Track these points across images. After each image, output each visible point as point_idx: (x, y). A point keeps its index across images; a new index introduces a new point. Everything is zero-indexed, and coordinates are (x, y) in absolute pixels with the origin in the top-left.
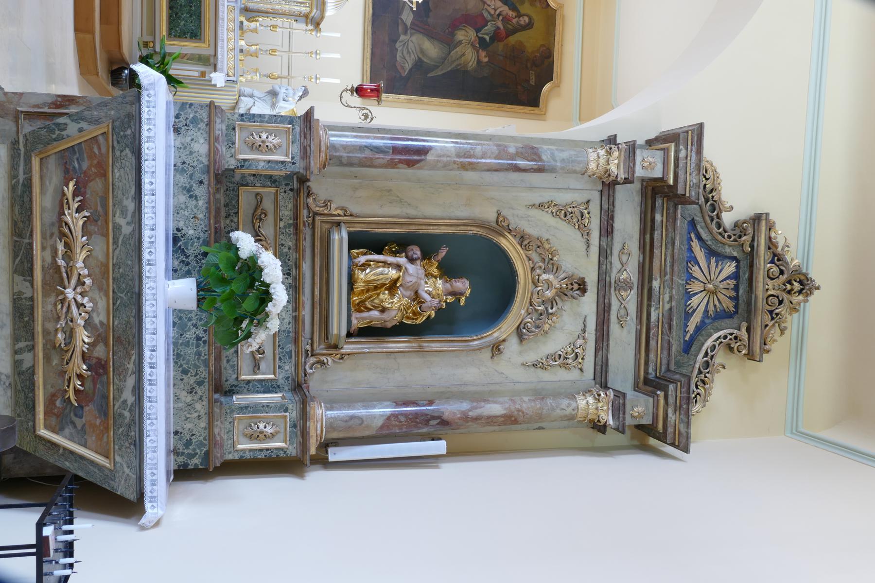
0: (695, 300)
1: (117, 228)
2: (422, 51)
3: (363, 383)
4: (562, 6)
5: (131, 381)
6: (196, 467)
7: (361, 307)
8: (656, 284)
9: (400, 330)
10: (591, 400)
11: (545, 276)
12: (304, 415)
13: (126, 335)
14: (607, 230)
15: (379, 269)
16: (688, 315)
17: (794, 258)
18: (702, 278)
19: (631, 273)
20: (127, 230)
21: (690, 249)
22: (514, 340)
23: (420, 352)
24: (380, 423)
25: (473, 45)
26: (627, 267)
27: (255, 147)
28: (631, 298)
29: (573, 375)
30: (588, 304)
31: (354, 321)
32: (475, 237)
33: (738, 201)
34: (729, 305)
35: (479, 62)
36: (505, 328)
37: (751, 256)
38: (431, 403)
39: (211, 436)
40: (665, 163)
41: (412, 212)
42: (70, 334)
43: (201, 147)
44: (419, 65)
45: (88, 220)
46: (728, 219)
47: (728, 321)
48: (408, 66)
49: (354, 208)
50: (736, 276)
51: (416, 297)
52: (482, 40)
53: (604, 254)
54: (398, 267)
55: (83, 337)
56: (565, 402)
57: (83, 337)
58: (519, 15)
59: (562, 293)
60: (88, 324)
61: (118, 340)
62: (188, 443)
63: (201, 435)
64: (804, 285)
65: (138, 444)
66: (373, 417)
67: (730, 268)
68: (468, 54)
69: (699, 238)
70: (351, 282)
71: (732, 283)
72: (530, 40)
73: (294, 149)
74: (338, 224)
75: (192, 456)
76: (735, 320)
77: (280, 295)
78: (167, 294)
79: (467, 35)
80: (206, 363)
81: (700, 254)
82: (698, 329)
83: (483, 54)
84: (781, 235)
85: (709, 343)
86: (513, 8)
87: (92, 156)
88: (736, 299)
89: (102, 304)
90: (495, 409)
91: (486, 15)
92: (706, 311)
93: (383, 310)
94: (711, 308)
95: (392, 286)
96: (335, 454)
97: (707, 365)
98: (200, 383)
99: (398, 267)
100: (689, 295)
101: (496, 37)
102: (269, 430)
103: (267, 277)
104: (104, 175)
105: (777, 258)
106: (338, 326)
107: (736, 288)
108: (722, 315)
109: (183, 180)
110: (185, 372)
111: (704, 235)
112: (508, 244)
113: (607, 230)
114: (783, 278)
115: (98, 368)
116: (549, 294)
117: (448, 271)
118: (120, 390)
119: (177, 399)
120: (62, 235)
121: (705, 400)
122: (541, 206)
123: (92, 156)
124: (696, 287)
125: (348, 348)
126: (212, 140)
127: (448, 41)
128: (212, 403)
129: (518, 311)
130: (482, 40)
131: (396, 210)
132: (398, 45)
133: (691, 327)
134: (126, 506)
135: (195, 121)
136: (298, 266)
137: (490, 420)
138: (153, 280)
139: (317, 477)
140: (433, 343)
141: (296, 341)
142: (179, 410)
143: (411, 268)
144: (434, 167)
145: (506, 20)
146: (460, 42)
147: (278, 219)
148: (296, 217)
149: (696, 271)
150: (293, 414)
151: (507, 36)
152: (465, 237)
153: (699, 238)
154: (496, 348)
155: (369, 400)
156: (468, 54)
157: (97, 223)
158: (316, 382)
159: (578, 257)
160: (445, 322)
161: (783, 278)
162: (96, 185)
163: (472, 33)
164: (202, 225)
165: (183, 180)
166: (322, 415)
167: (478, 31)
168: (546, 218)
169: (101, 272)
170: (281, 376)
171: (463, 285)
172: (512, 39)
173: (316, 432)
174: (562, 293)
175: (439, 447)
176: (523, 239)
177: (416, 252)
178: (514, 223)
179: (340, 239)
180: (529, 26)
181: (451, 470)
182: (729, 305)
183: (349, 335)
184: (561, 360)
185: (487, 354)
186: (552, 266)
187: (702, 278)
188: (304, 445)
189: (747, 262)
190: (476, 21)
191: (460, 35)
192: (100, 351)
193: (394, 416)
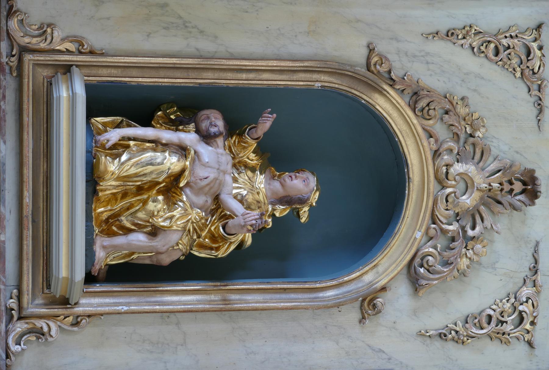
7: (112, 226)
9: (187, 269)
11: (458, 168)
15: (146, 154)
22: (402, 288)
23: (225, 310)
32: (327, 93)
36: (386, 266)
41: (206, 46)
49: (96, 39)
51: (217, 208)
54: (182, 150)
59: (492, 200)
74: (67, 69)
93: (155, 232)
95: (171, 187)
99: (182, 150)
106: (69, 265)
112: (390, 107)
116: (468, 201)
117: (276, 157)
122: (450, 34)
125: (88, 304)
129: (409, 233)
131: (175, 42)
140: (249, 294)
143: (206, 152)
154: (369, 304)
160: (271, 255)
171: (304, 184)
174: (492, 200)
177: (215, 121)
179: (70, 97)
185: (354, 314)
186: (471, 146)
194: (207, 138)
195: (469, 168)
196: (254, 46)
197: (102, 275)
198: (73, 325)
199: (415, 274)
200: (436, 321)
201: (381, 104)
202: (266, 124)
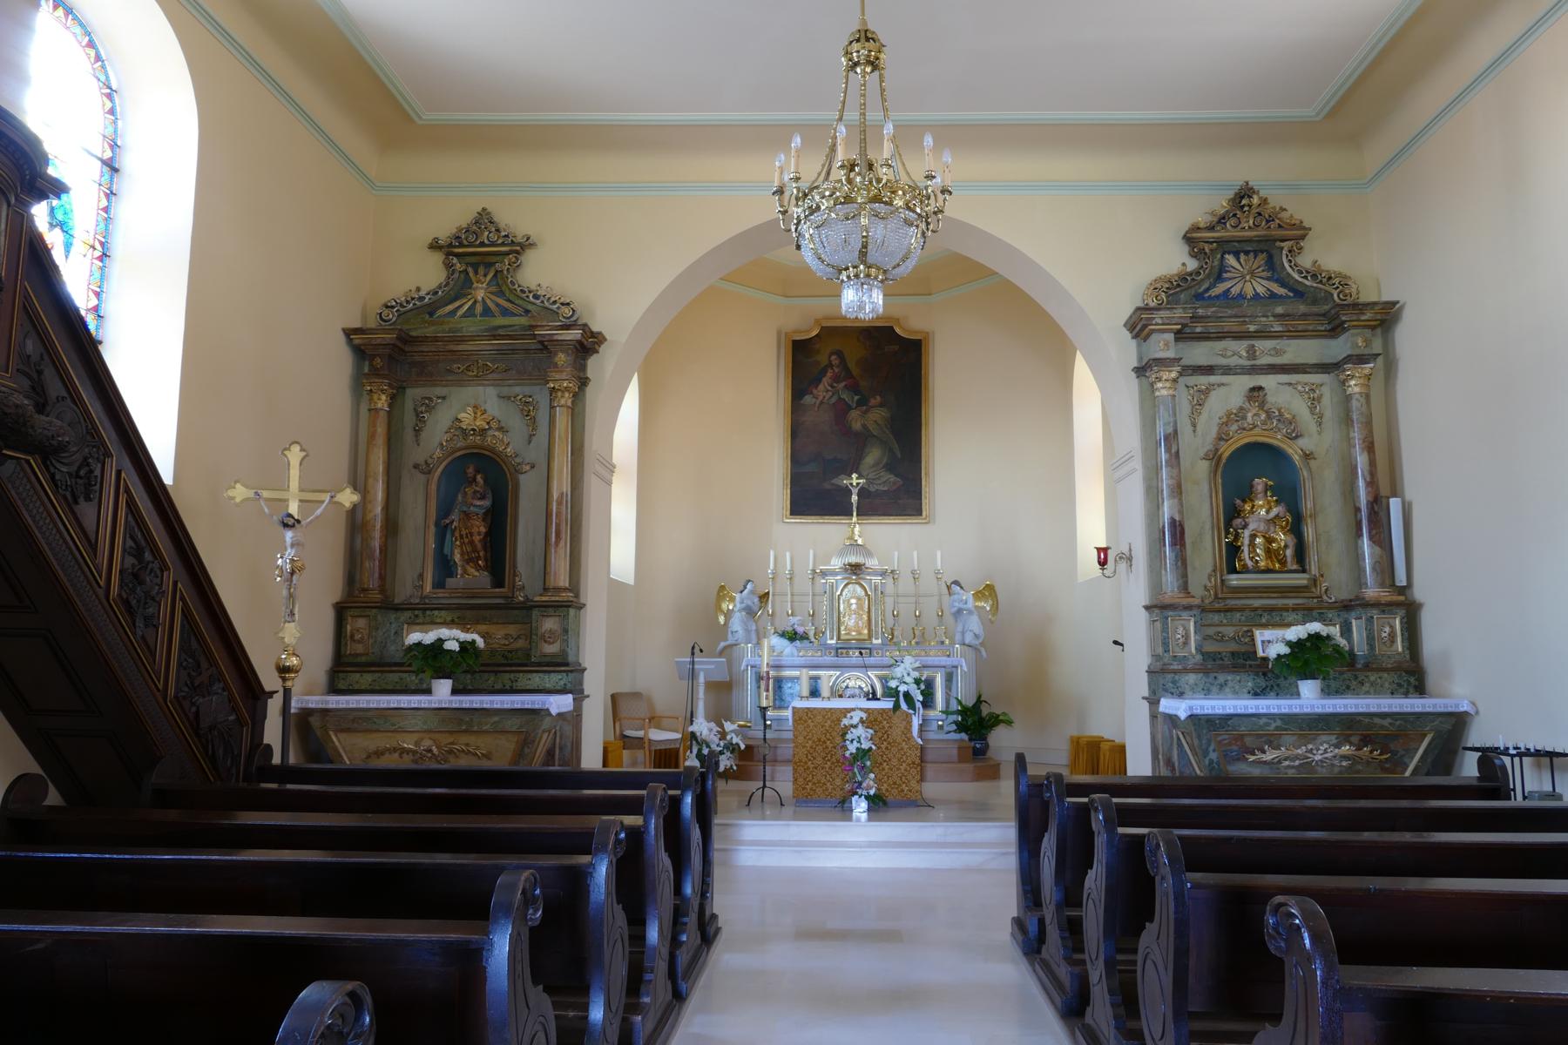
0: (1260, 290)
1: (1277, 728)
2: (876, 464)
3: (1336, 557)
4: (817, 321)
5: (1377, 720)
6: (1413, 676)
7: (1283, 562)
8: (1252, 328)
9: (1296, 528)
10: (1353, 383)
11: (1249, 419)
12: (1376, 605)
13: (1346, 725)
14: (1209, 370)
15: (1254, 552)
16: (1273, 295)
17: (1221, 203)
18: (1240, 285)
19: (1241, 347)
20: (1279, 723)
21: (1217, 297)
22: (1300, 442)
23: (1314, 516)
24: (1377, 549)
25: (865, 412)
26: (1235, 351)
27: (1186, 643)
28: (1262, 345)
29: (1326, 393)
30: (1268, 382)
31: (1295, 567)
32: (1223, 472)
33: (1175, 260)
34: (1262, 257)
35: (881, 405)
36: (1293, 451)
37: (1220, 242)
38: (1358, 510)
39: (1392, 670)
40: (1163, 331)
41: (1208, 526)
42: (1344, 757)
43: (1192, 678)
44: (890, 468)
45: (1270, 743)
46: (1192, 265)
47: (1276, 259)
48: (892, 478)
49: (1209, 569)
50: (1237, 255)
51: (1273, 521)
52: (860, 403)
53: (1228, 371)
54: (1253, 537)
55: (1346, 749)
56: (1354, 404)
57: (1346, 749)
58: (830, 365)
59: (1262, 405)
60: (1337, 746)
61: (1349, 728)
62: (1400, 685)
63: (1394, 677)
64: (1245, 192)
65: (1419, 715)
66: (1372, 555)
67: (1231, 260)
68: (874, 418)
69: (1208, 290)
70: (1268, 571)
71: (1242, 257)
72: (855, 353)
73: (1185, 615)
74: (1223, 581)
75: (1409, 683)
76: (1274, 252)
77: (1315, 627)
78: (1309, 697)
79: (856, 421)
80: (1341, 673)
81: (1220, 288)
82: (1283, 285)
83: (873, 402)
84: (1202, 220)
85: (1296, 276)
86: (823, 372)
87: (1230, 744)
88: (1256, 253)
89: (1324, 738)
90: (1361, 460)
91: (834, 400)
92: (1267, 279)
93: (1286, 546)
94: (1264, 274)
95: (1269, 540)
96: (1401, 580)
97: (1314, 276)
98: (1356, 678)
99: (1253, 537)
100: (1256, 296)
101: (854, 388)
102: (1387, 629)
103: (1303, 635)
104: (1242, 736)
105: (1222, 220)
106: (1300, 580)
107: (1247, 253)
108: (1272, 265)
109: (1215, 689)
110: (1348, 687)
111: (1206, 285)
112: (1227, 450)
113: (1209, 370)
114: (1239, 213)
115: (1366, 740)
116: (1263, 416)
117: (1248, 495)
118: (1382, 727)
119: (1368, 693)
120: (1280, 762)
121: (1346, 277)
122: (1194, 425)
123: (1230, 744)
124: (1249, 292)
125: (1314, 570)
126: (1186, 671)
127: (861, 441)
128: (1373, 670)
129: (1277, 440)
130: (860, 403)
131: (1208, 537)
132: (872, 489)
133: (1282, 291)
134: (1458, 722)
135: (1174, 682)
136: (1256, 609)
137: (1372, 463)
138: (1301, 706)
139: (1419, 593)
140: (1307, 506)
141: (1311, 609)
142: (1377, 691)
143: (1252, 526)
144: (1181, 512)
145: (836, 379)
146: (864, 426)
147: (1221, 624)
148: (1219, 611)
149: (1235, 291)
150: (1375, 613)
151: (852, 376)
152: (1223, 485)
153: (1208, 290)
154: (1307, 456)
155: (1358, 557)
156: (874, 418)
157: (1273, 741)
158: (1341, 593)
159: (1230, 394)
160: (1288, 494)
161: (1239, 213)
162: (1248, 741)
163: (854, 414)
164: (1244, 677)
165: (1215, 689)
166: (1372, 592)
167: (850, 408)
168: (1202, 420)
169: (1304, 739)
170: (1337, 620)
171: (1259, 484)
172: (855, 371)
173: (1385, 595)
174: (1262, 405)
175: (1395, 503)
176: (1222, 438)
177: (1238, 522)
178: (1209, 447)
179: (1234, 580)
180: (839, 354)
181: (1410, 491)
182: (1262, 257)
183: (1304, 571)
184: (1314, 402)
185: (1312, 462)
186: (1240, 414)
187: (1240, 285)
188: (1398, 604)
189: (1225, 246)
190: (841, 410)
191: (857, 426)
192: (1355, 739)
193: (1371, 538)
194: (1245, 526)
195: (1250, 415)
196: (1206, 506)
197: (1175, 471)
198: (905, 221)
199: (1295, 436)
200: (1313, 428)
201: (1226, 455)
202: (1238, 502)
